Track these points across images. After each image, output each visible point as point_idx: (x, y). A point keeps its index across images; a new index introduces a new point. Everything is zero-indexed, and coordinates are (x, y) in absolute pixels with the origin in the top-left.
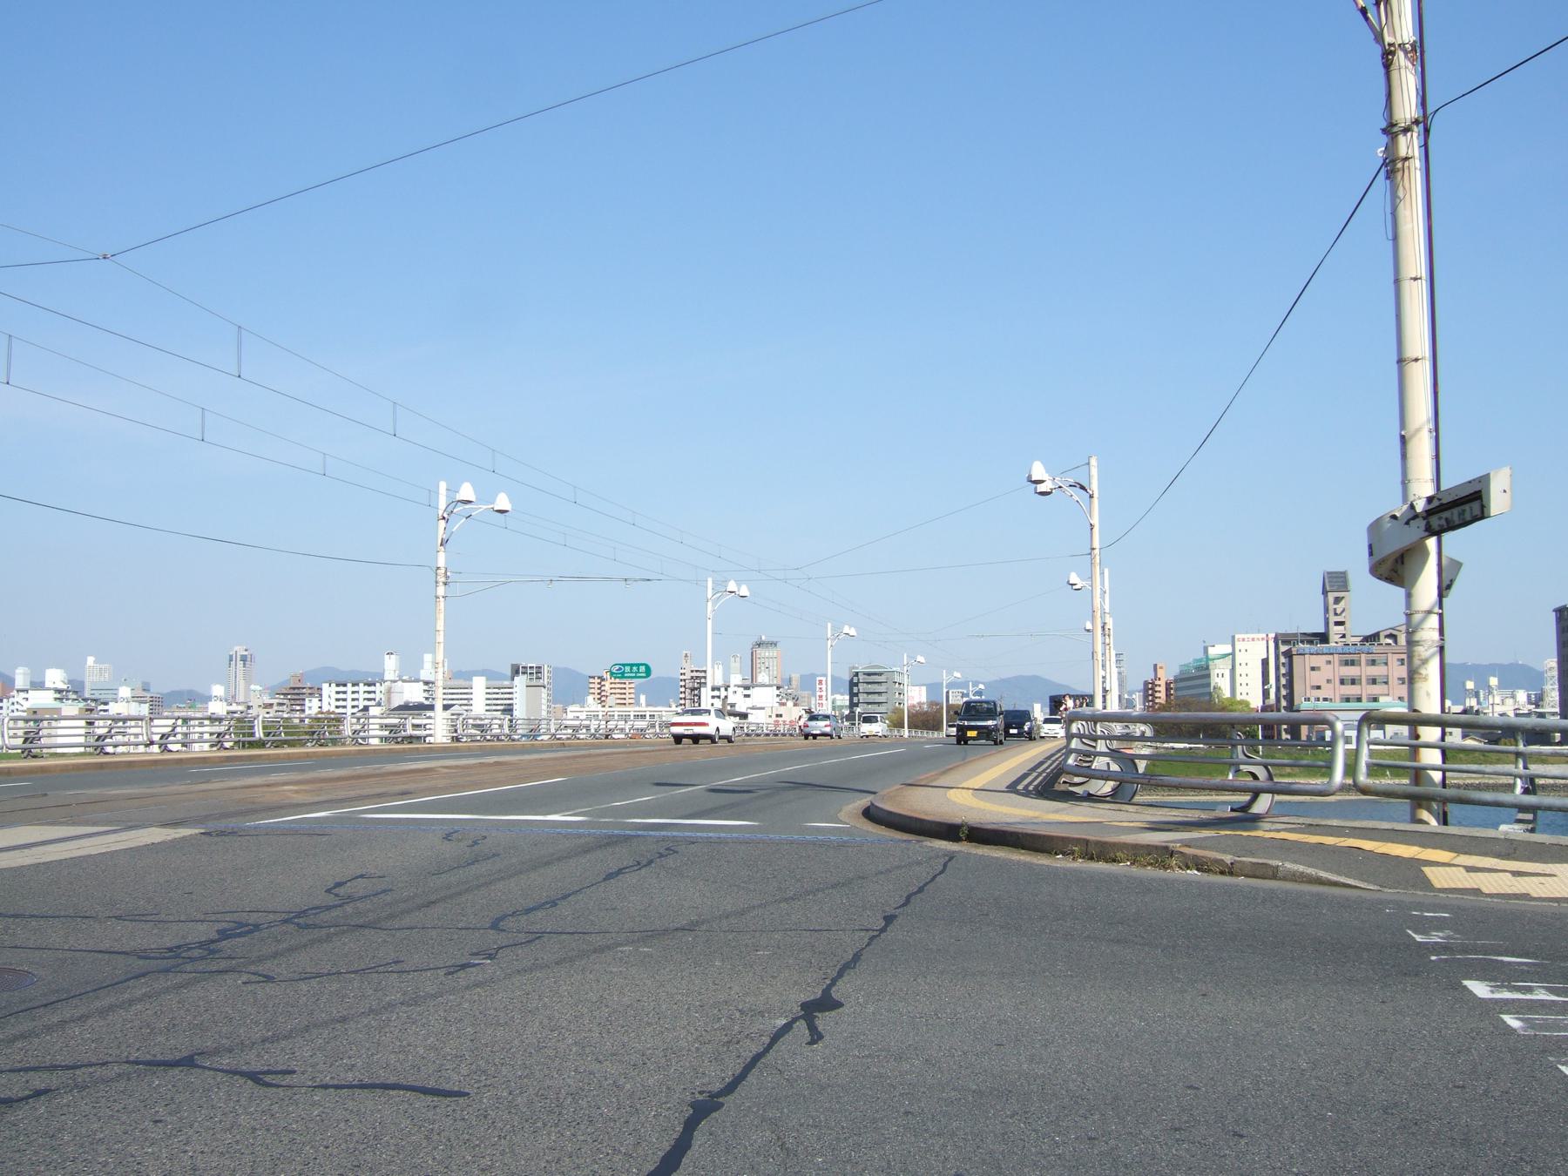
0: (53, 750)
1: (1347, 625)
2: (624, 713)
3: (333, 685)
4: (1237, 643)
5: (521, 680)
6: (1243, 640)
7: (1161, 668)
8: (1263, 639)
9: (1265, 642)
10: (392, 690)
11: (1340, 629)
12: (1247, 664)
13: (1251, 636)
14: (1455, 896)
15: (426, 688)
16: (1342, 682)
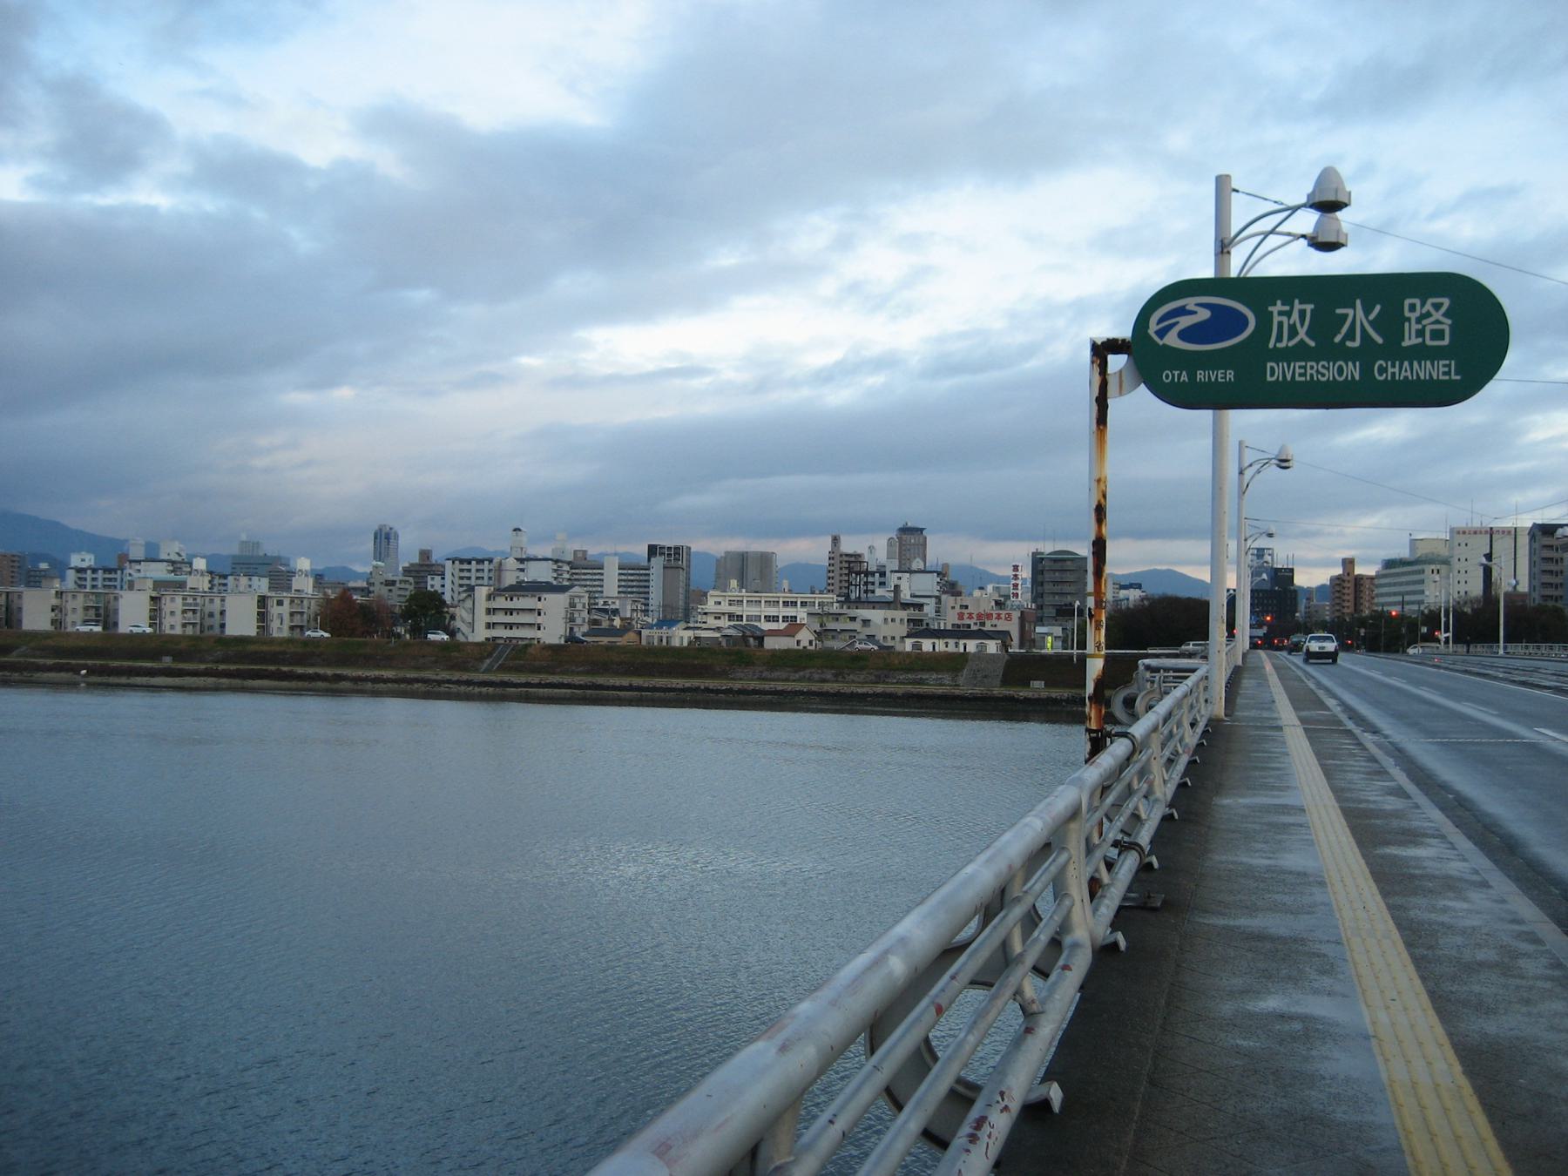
2: (774, 599)
3: (457, 562)
5: (658, 562)
10: (503, 568)
12: (1466, 545)
14: (1476, 740)
15: (555, 567)
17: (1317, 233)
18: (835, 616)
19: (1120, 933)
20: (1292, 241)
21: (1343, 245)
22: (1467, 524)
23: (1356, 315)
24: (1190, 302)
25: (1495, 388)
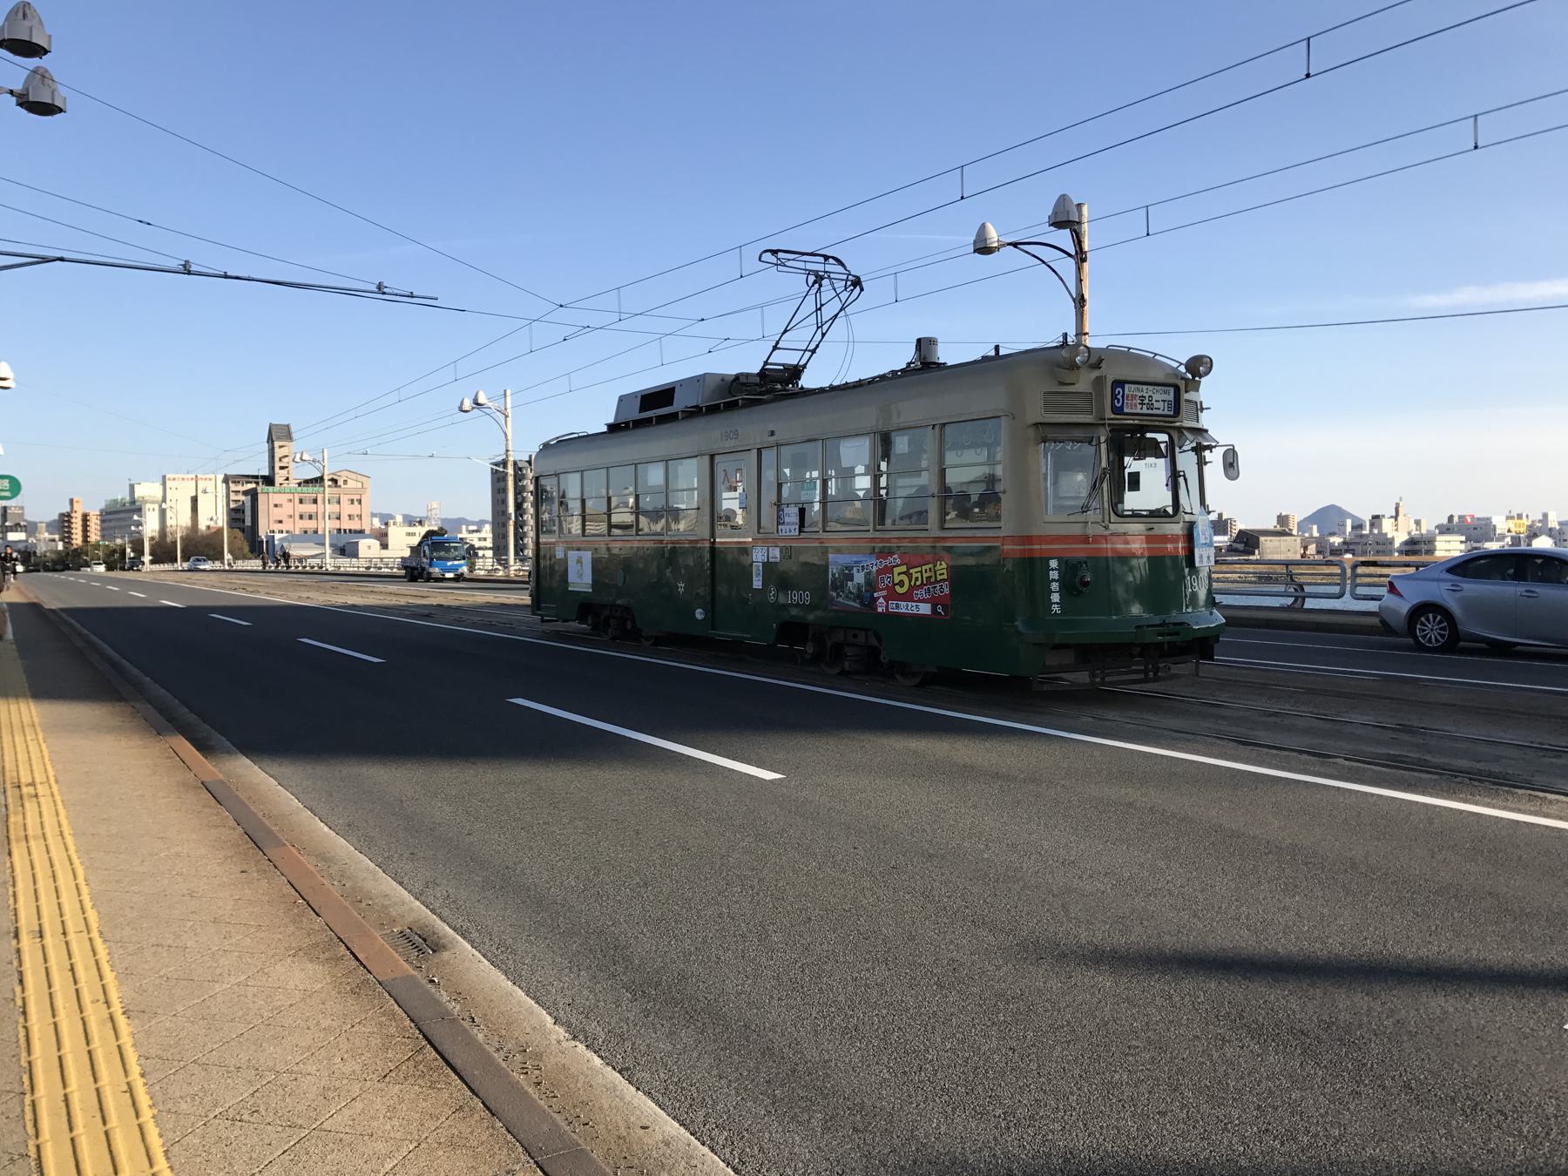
4: (168, 483)
6: (174, 479)
7: (77, 502)
8: (192, 479)
9: (194, 481)
11: (284, 472)
13: (181, 476)
16: (301, 517)
17: (27, 90)
21: (61, 110)
22: (1409, 533)
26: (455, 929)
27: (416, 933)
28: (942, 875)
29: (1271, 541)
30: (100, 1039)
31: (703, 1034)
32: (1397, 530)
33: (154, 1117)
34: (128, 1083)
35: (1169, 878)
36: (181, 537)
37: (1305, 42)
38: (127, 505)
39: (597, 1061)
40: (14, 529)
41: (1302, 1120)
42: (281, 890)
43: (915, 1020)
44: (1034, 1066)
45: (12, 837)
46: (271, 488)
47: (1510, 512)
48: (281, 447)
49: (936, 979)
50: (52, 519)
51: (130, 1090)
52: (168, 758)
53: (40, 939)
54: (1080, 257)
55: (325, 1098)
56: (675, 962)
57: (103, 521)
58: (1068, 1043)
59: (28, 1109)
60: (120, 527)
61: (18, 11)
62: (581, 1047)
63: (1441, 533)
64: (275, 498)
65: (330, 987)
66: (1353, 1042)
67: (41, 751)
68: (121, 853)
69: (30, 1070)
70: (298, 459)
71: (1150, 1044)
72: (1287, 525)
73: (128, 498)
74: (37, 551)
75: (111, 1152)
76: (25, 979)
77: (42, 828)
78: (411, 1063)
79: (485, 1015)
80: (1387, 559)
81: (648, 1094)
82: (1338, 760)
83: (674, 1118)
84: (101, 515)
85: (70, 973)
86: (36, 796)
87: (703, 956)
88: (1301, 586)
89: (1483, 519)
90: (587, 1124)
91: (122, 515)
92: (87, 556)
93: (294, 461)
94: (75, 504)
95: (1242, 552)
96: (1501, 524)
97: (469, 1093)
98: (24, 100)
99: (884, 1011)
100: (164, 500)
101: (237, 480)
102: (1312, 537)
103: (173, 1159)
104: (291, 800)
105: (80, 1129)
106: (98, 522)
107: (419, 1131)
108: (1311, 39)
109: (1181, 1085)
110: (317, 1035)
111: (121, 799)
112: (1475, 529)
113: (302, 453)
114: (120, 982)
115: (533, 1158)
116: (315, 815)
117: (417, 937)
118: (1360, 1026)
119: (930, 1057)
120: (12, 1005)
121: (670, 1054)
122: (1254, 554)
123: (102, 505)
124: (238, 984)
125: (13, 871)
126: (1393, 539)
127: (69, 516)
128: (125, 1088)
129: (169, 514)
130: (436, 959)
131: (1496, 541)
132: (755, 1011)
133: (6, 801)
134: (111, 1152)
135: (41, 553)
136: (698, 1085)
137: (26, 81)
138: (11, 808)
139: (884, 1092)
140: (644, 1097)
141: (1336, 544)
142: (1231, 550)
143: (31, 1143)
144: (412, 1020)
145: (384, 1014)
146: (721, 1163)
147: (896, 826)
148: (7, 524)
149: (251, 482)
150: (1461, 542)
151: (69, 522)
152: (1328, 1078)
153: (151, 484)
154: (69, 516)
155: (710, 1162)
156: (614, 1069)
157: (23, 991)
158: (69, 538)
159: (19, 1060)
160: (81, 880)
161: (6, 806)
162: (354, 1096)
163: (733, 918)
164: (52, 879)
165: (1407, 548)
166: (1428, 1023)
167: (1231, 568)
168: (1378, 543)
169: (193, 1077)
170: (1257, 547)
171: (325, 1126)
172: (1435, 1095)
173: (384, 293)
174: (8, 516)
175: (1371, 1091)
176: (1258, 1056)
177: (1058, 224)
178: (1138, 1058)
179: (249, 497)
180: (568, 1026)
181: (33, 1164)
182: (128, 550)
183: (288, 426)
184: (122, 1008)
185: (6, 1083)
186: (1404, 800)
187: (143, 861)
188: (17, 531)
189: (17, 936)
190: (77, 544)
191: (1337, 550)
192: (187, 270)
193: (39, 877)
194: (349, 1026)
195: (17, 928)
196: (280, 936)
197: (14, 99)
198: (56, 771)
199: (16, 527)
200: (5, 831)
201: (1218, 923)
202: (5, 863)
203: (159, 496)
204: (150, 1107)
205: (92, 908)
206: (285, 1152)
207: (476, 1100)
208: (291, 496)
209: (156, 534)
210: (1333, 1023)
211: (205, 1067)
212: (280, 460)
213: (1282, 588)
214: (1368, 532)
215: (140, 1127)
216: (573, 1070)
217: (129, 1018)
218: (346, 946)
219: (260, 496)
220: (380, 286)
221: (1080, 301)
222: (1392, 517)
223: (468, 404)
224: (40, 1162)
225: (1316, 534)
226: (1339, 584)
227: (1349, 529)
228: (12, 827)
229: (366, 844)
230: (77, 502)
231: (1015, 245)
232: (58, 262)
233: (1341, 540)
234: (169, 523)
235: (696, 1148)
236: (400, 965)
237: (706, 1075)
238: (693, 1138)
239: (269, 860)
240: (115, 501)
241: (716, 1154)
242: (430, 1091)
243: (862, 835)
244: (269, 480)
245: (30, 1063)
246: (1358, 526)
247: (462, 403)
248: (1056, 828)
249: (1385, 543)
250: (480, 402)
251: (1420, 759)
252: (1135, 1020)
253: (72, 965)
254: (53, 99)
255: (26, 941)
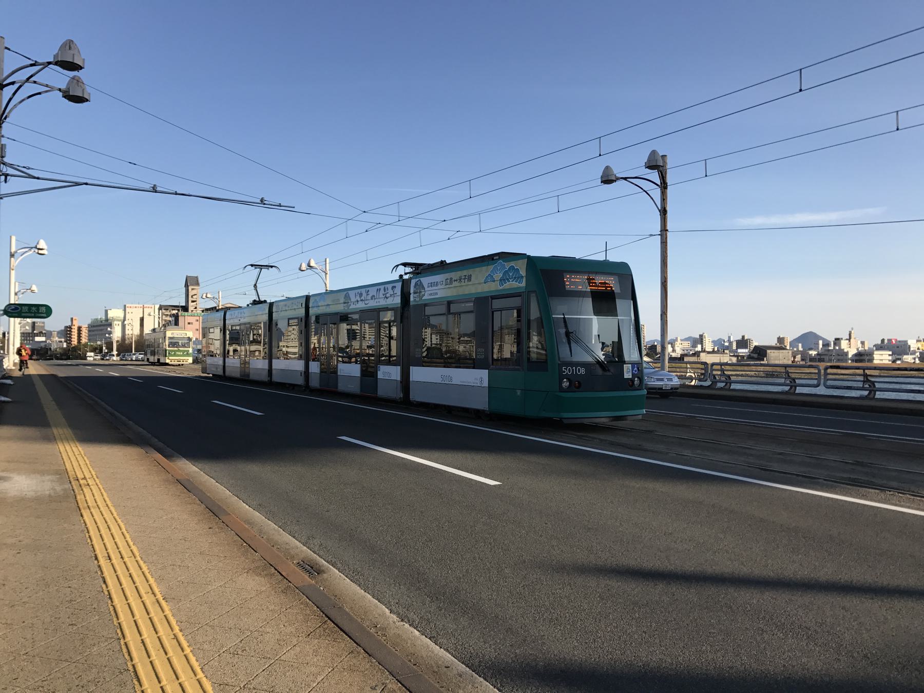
0: (593, 354)
1: (197, 302)
4: (127, 309)
6: (131, 307)
7: (75, 320)
8: (141, 307)
9: (142, 309)
17: (69, 89)
18: (357, 291)
19: (5, 367)
20: (44, 68)
21: (87, 100)
22: (858, 349)
23: (34, 308)
24: (12, 306)
25: (50, 318)
26: (328, 562)
27: (307, 564)
28: (597, 539)
29: (774, 352)
30: (154, 612)
31: (473, 621)
32: (850, 347)
33: (191, 651)
34: (174, 634)
35: (726, 544)
36: (135, 341)
37: (799, 72)
38: (103, 322)
39: (417, 633)
40: (39, 335)
41: (809, 673)
42: (233, 538)
43: (589, 616)
44: (657, 641)
45: (81, 507)
46: (186, 313)
47: (919, 337)
48: (193, 289)
49: (599, 595)
50: (60, 329)
51: (176, 637)
52: (155, 466)
53: (109, 561)
54: (664, 186)
55: (279, 645)
56: (452, 583)
57: (89, 331)
58: (676, 630)
59: (124, 647)
60: (99, 334)
61: (66, 45)
62: (407, 626)
63: (877, 349)
64: (189, 319)
65: (271, 589)
66: (835, 634)
67: (85, 461)
68: (141, 516)
69: (120, 627)
70: (204, 297)
71: (721, 632)
72: (783, 343)
73: (104, 318)
74: (52, 348)
75: (173, 668)
76: (106, 581)
77: (96, 502)
78: (321, 629)
79: (352, 608)
80: (844, 364)
81: (447, 650)
82: (820, 480)
83: (463, 663)
84: (89, 327)
85: (130, 578)
86: (88, 485)
87: (467, 580)
88: (794, 380)
89: (903, 341)
90: (416, 665)
91: (102, 328)
92: (80, 351)
93: (202, 297)
94: (74, 321)
95: (756, 359)
96: (913, 344)
97: (355, 645)
98: (67, 94)
99: (572, 611)
100: (124, 320)
101: (166, 308)
102: (798, 350)
103: (206, 672)
104: (225, 491)
105: (154, 657)
106: (87, 331)
107: (332, 662)
108: (802, 70)
109: (740, 653)
110: (268, 614)
111: (134, 488)
112: (898, 347)
113: (207, 293)
114: (158, 584)
115: (395, 678)
116: (240, 499)
117: (307, 566)
118: (839, 625)
119: (599, 635)
120: (103, 594)
121: (456, 630)
122: (763, 360)
123: (89, 322)
124: (221, 586)
125: (86, 525)
126: (848, 352)
127: (70, 327)
128: (173, 637)
129: (127, 327)
130: (320, 578)
131: (911, 355)
132: (500, 609)
133: (72, 487)
134: (173, 668)
135: (54, 349)
136: (473, 646)
137: (68, 84)
138: (76, 491)
139: (576, 652)
140: (444, 652)
141: (813, 355)
142: (750, 357)
143: (129, 664)
144: (318, 607)
145: (302, 603)
146: (491, 686)
147: (568, 513)
148: (35, 332)
149: (175, 310)
150: (889, 355)
151: (70, 331)
152: (822, 652)
153: (117, 310)
154: (70, 327)
155: (485, 686)
156: (426, 637)
157: (107, 587)
158: (70, 340)
159: (113, 622)
160: (124, 530)
161: (73, 490)
162: (295, 644)
163: (482, 560)
164: (108, 529)
165: (857, 358)
166: (876, 624)
167: (750, 368)
168: (838, 355)
169: (207, 632)
170: (766, 356)
171: (282, 658)
172: (882, 661)
173: (264, 204)
174: (36, 327)
175: (846, 659)
176: (782, 639)
177: (651, 166)
178: (715, 639)
179: (173, 318)
180: (398, 615)
181: (132, 674)
182: (104, 348)
183: (197, 277)
184: (162, 596)
185: (109, 634)
186: (859, 504)
187: (154, 521)
188: (40, 336)
189: (96, 558)
190: (74, 344)
191: (813, 359)
192: (154, 190)
193: (101, 528)
194: (285, 609)
195: (96, 554)
196: (237, 562)
197: (61, 93)
198: (95, 472)
199: (40, 334)
200: (76, 504)
201: (755, 568)
202: (80, 520)
203: (122, 316)
204: (189, 646)
205: (133, 545)
206: (263, 670)
207: (360, 648)
208: (198, 318)
209: (120, 339)
210: (824, 623)
211: (212, 627)
212: (192, 297)
213: (782, 381)
214: (832, 348)
215: (185, 656)
216: (404, 637)
217: (167, 602)
218: (274, 568)
219: (180, 318)
220: (262, 200)
221: (664, 212)
222: (847, 339)
223: (304, 267)
224: (136, 673)
225: (801, 349)
226: (816, 379)
227: (821, 346)
228: (79, 502)
229: (271, 516)
230: (75, 320)
231: (625, 179)
232: (84, 185)
233: (816, 353)
234: (127, 332)
235: (476, 678)
236: (304, 579)
237: (477, 641)
238: (474, 673)
239: (223, 522)
240: (97, 319)
241: (487, 681)
242: (334, 643)
243: (549, 517)
244: (185, 309)
245: (119, 623)
246: (826, 344)
247: (301, 266)
248: (659, 515)
249: (843, 355)
250: (311, 265)
251: (868, 480)
252: (712, 619)
253: (130, 574)
254: (83, 94)
255: (103, 562)
